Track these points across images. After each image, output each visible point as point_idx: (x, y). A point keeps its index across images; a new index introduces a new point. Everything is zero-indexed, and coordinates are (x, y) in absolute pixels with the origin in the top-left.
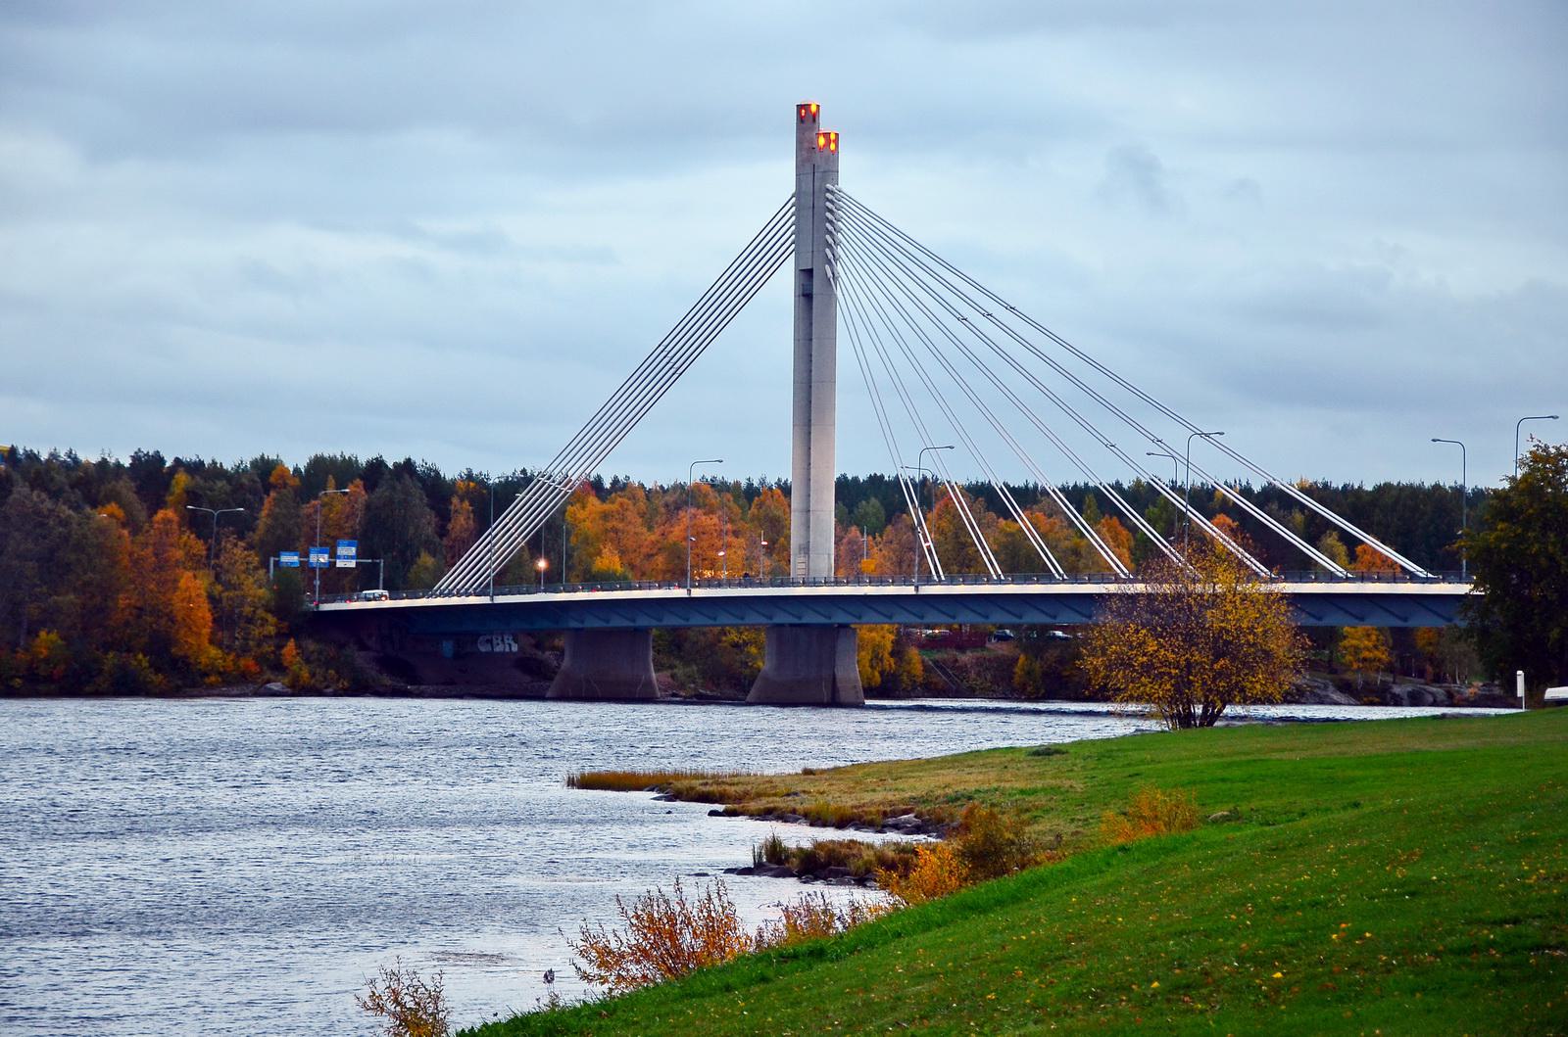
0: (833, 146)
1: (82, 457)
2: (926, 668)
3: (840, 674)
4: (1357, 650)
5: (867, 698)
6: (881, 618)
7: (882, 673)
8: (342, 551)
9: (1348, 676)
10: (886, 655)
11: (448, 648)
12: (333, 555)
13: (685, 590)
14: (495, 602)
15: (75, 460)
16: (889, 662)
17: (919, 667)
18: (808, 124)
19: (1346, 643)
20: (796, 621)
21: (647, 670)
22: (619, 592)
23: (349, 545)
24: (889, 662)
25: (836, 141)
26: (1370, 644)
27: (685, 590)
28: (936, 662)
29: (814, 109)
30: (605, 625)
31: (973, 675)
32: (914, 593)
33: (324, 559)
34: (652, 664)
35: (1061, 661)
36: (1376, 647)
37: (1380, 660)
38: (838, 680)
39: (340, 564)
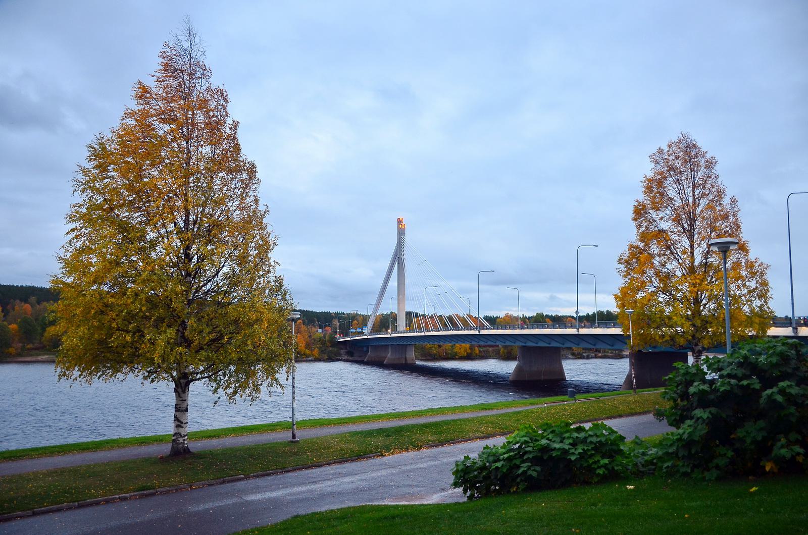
0: (403, 227)
2: (480, 351)
3: (407, 356)
5: (417, 359)
7: (467, 353)
9: (574, 351)
12: (362, 329)
13: (791, 329)
16: (469, 351)
17: (478, 351)
24: (469, 351)
27: (791, 329)
28: (483, 351)
29: (401, 219)
32: (577, 333)
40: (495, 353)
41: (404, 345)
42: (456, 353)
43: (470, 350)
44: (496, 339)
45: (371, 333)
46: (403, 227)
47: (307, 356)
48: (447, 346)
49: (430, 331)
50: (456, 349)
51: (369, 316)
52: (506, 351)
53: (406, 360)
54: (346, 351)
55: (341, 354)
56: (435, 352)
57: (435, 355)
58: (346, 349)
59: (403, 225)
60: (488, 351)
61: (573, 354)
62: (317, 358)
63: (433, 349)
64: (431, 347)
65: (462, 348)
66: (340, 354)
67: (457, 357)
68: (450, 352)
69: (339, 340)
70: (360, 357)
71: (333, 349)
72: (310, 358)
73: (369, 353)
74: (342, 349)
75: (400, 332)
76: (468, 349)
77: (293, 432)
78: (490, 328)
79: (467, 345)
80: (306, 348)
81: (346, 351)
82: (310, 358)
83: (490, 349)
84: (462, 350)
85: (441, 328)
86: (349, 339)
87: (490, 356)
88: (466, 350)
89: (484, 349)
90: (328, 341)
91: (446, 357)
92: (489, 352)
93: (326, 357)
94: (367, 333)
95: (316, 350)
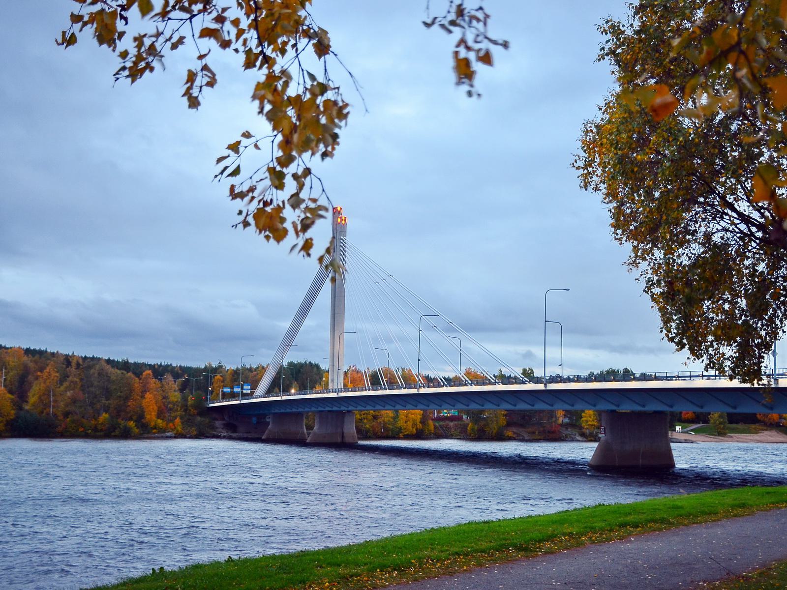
0: (343, 222)
1: (130, 361)
2: (435, 427)
3: (346, 431)
4: (587, 421)
5: (360, 439)
6: (452, 407)
7: (416, 430)
8: (245, 387)
9: (584, 430)
10: (418, 423)
11: (254, 420)
12: (242, 388)
13: (543, 385)
14: (548, 388)
15: (128, 361)
16: (420, 426)
17: (433, 427)
18: (337, 214)
19: (583, 419)
20: (331, 409)
21: (302, 428)
22: (614, 383)
23: (248, 385)
24: (420, 426)
25: (345, 220)
26: (591, 419)
27: (543, 385)
28: (440, 426)
29: (339, 209)
30: (339, 409)
31: (453, 430)
32: (544, 389)
33: (239, 390)
34: (305, 427)
35: (484, 425)
36: (593, 421)
37: (594, 425)
38: (345, 434)
39: (244, 392)
40: (459, 431)
41: (342, 411)
42: (400, 429)
43: (421, 425)
44: (396, 402)
45: (269, 392)
46: (343, 222)
47: (165, 431)
48: (387, 414)
49: (366, 390)
50: (401, 423)
51: (264, 369)
52: (476, 427)
53: (343, 437)
54: (224, 422)
55: (217, 428)
56: (368, 426)
57: (367, 431)
58: (224, 419)
59: (343, 218)
60: (448, 428)
61: (583, 435)
62: (180, 434)
63: (365, 421)
64: (361, 420)
65: (409, 420)
66: (213, 428)
67: (401, 435)
68: (391, 427)
69: (211, 405)
70: (247, 433)
71: (203, 419)
72: (168, 434)
73: (270, 426)
74: (217, 419)
75: (257, 397)
76: (418, 423)
77: (138, 542)
78: (496, 382)
79: (416, 414)
80: (158, 417)
81: (224, 422)
82: (168, 434)
83: (451, 424)
84: (410, 424)
85: (443, 382)
86: (238, 402)
87: (452, 435)
88: (414, 424)
89: (441, 423)
90: (192, 406)
91: (385, 435)
92: (450, 428)
93: (195, 433)
94: (260, 396)
95: (178, 420)
